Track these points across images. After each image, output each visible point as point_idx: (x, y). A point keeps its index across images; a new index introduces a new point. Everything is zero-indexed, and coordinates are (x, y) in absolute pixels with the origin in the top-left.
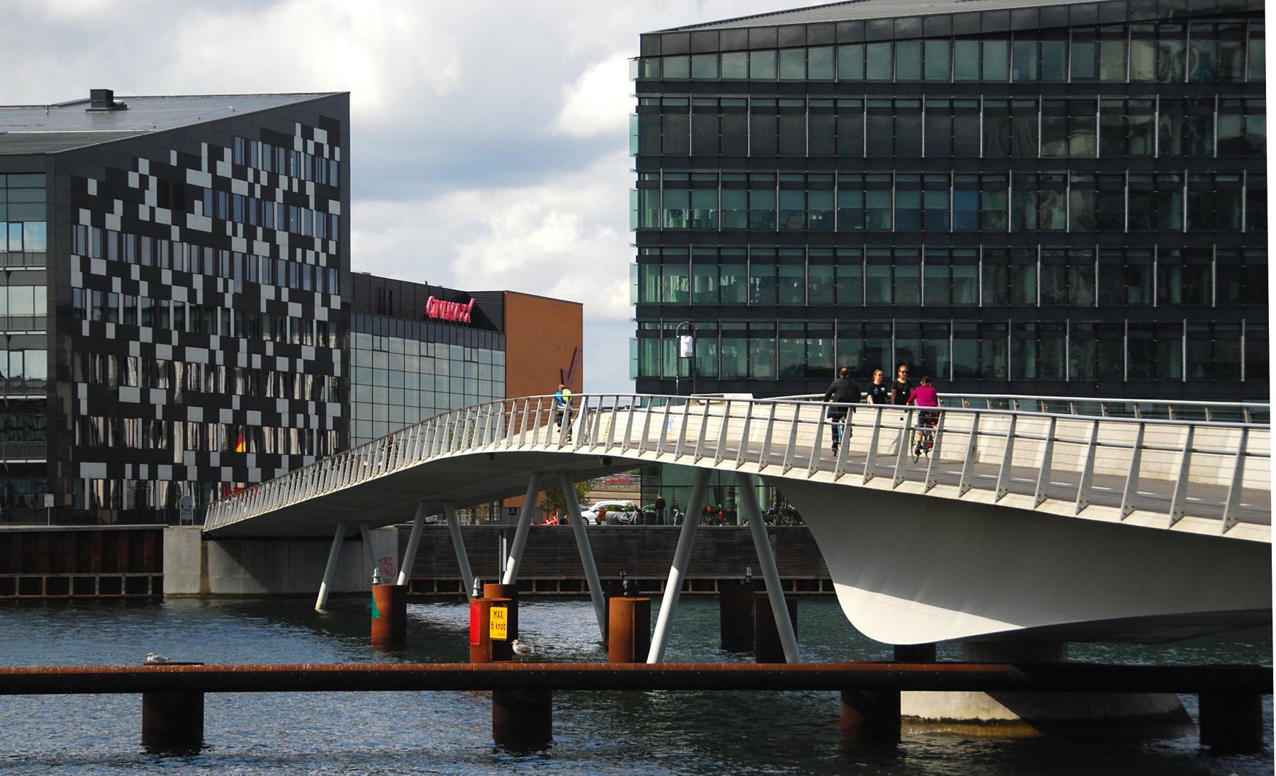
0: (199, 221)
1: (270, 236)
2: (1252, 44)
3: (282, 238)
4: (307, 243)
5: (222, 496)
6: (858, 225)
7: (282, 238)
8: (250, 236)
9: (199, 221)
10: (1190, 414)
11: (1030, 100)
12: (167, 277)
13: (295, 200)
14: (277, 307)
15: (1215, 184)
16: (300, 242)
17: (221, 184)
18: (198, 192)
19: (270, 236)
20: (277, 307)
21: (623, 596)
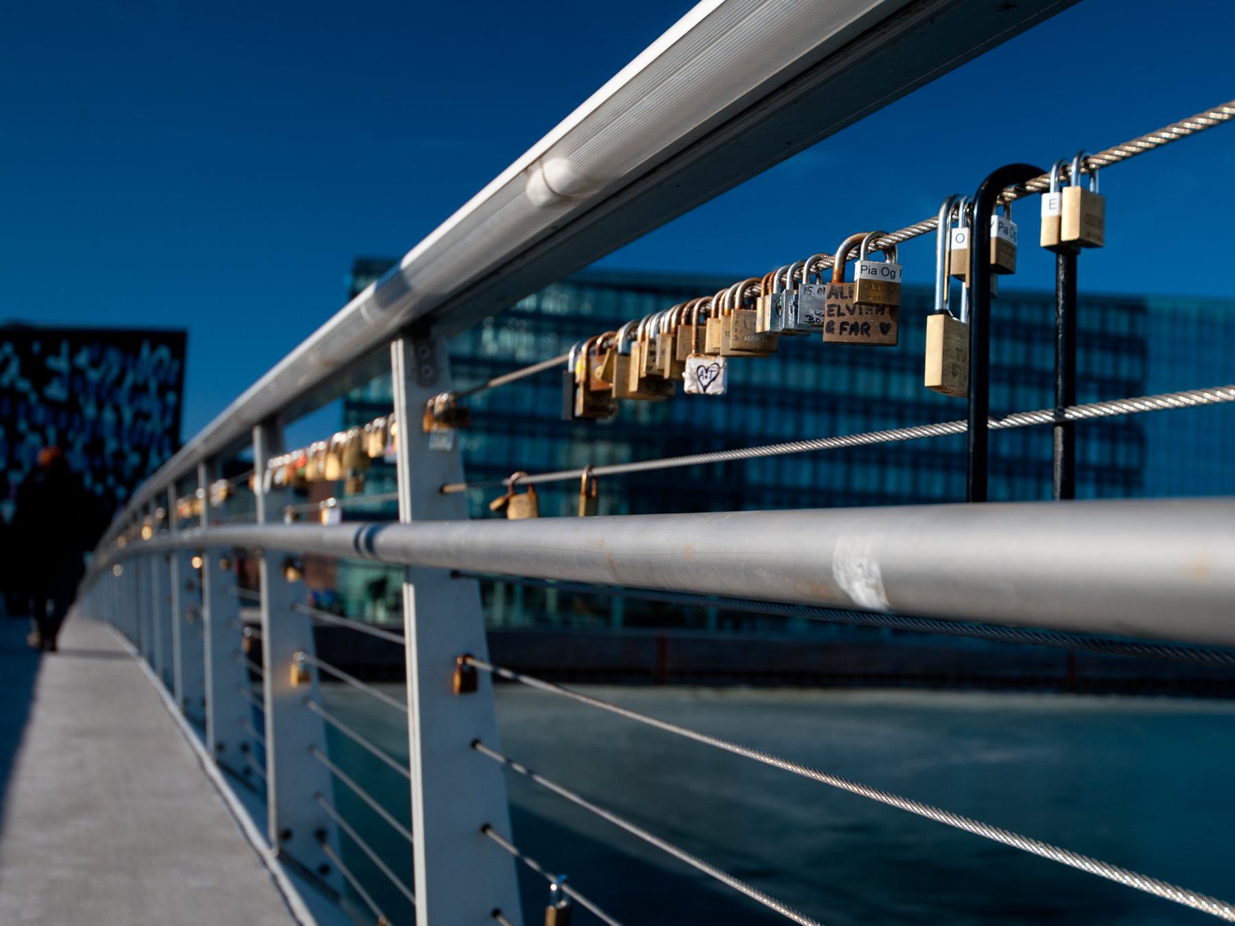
0: (56, 391)
1: (117, 409)
2: (913, 334)
3: (128, 415)
4: (147, 417)
5: (958, 318)
6: (456, 482)
7: (128, 415)
8: (100, 406)
9: (56, 391)
10: (834, 476)
11: (897, 338)
12: (22, 426)
13: (139, 390)
14: (120, 456)
15: (947, 300)
16: (142, 416)
17: (76, 372)
18: (56, 374)
19: (117, 409)
20: (120, 456)
21: (1096, 164)
